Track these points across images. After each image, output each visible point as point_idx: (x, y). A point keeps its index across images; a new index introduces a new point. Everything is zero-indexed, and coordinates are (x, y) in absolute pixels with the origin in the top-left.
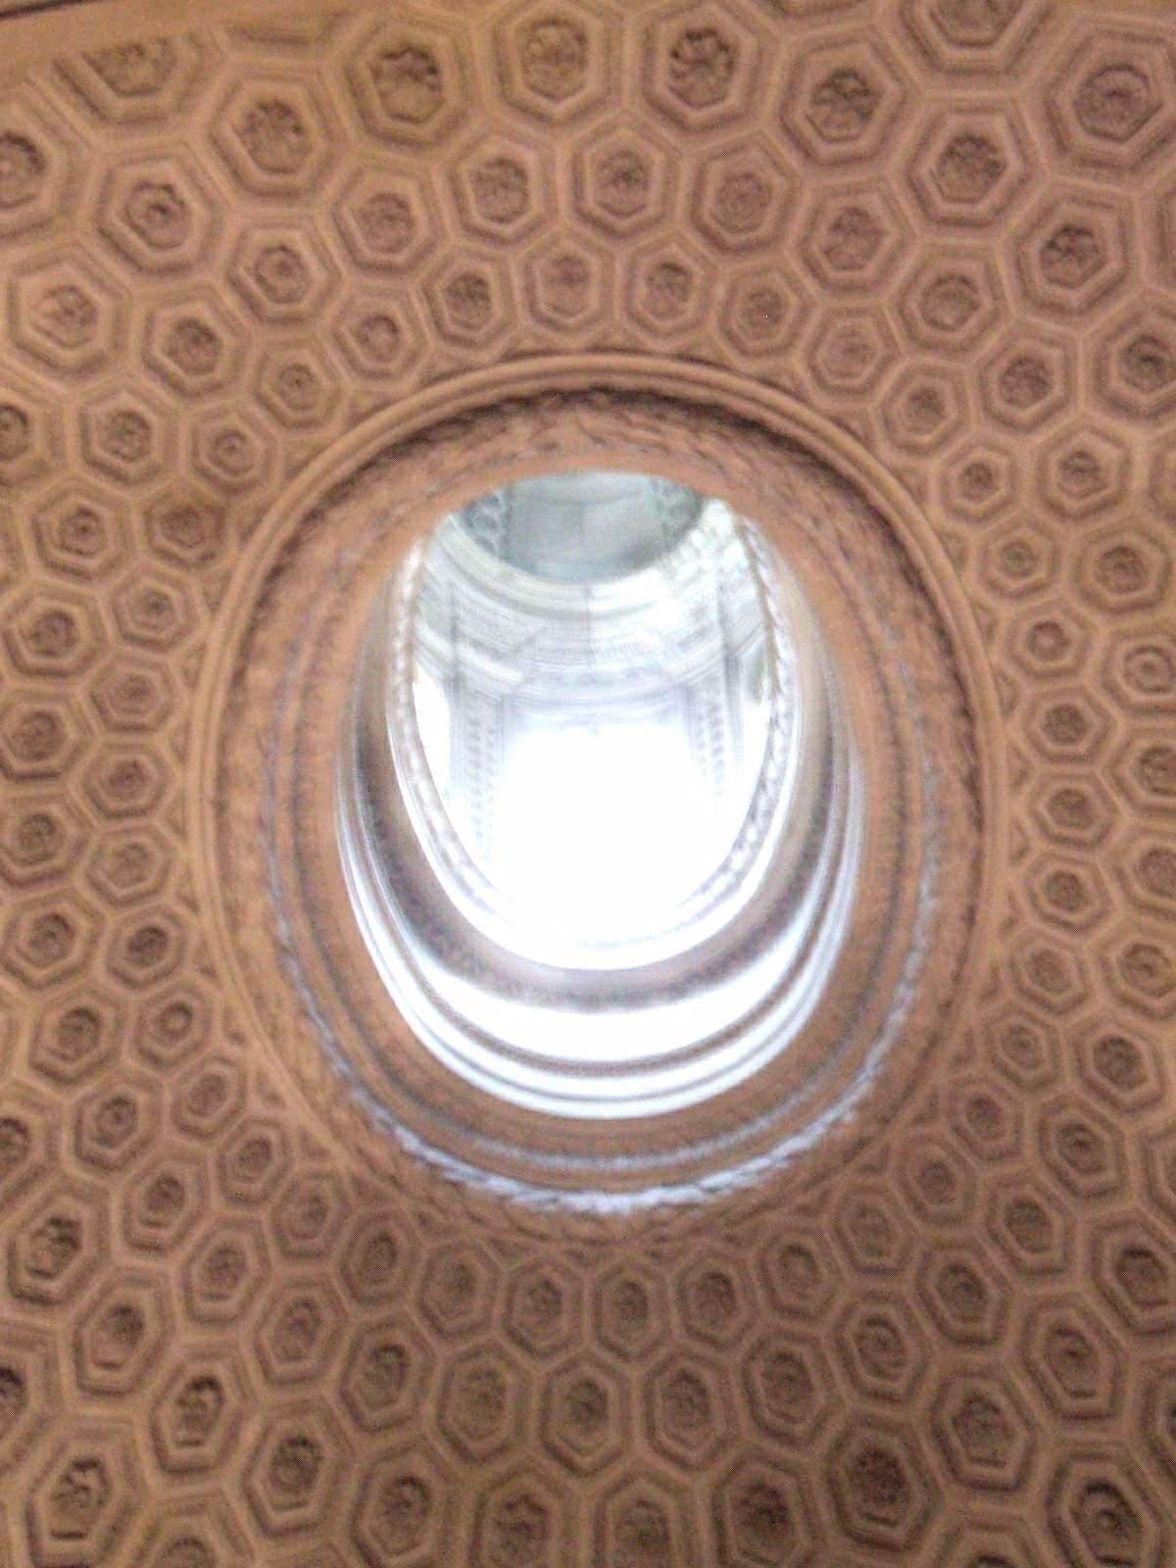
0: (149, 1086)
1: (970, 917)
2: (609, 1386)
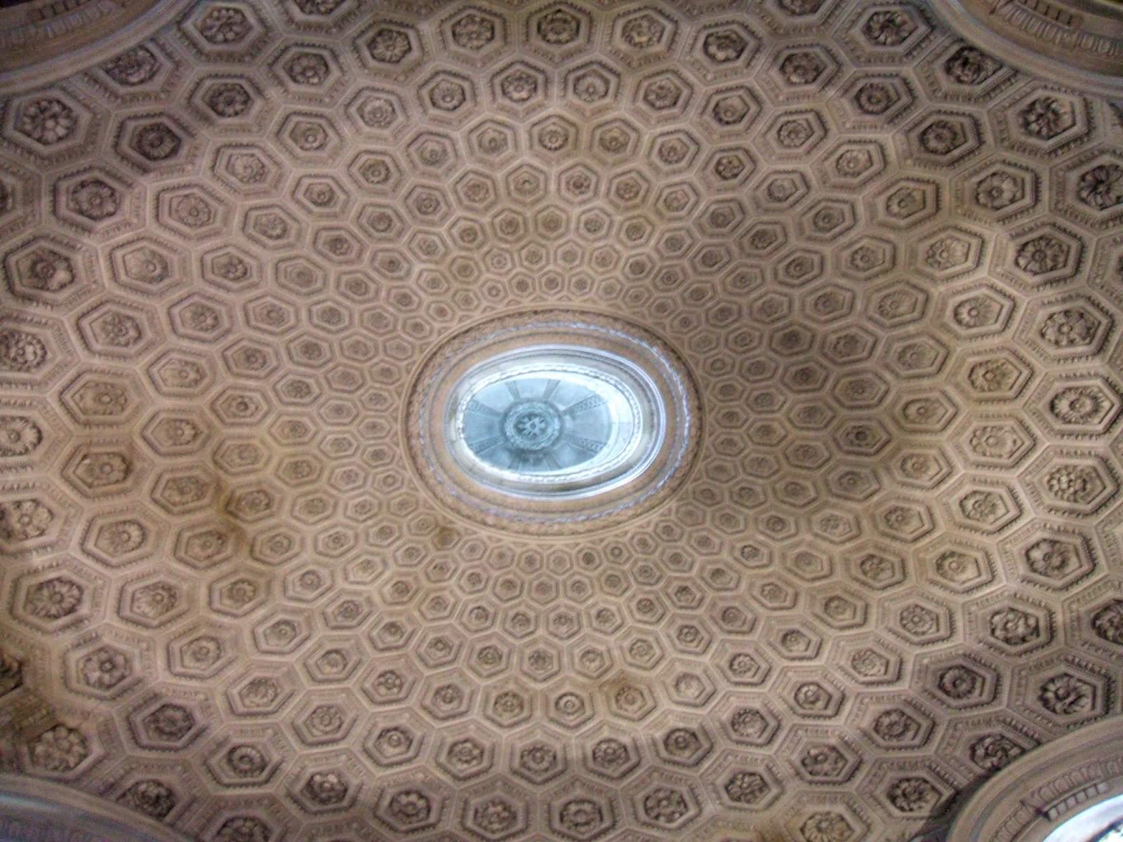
0: (635, 562)
1: (583, 313)
2: (759, 424)
